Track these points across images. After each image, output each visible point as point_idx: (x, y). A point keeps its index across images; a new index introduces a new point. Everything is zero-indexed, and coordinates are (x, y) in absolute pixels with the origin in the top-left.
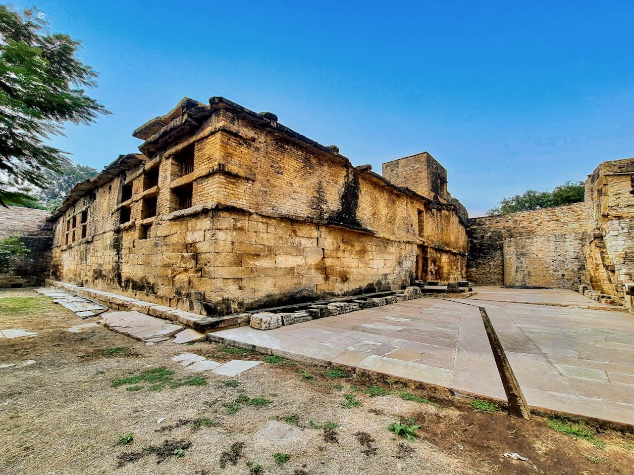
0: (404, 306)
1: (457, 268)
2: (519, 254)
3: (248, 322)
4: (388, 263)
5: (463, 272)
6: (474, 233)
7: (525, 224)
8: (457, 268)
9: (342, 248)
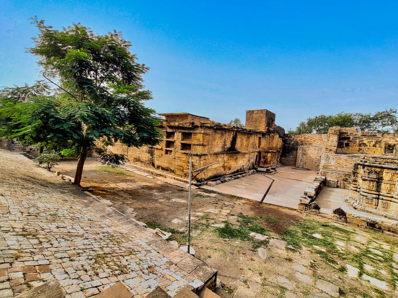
0: (249, 178)
1: (275, 158)
2: (303, 153)
3: (207, 184)
4: (245, 162)
5: (278, 159)
6: (286, 141)
7: (309, 140)
8: (275, 158)
9: (230, 159)
